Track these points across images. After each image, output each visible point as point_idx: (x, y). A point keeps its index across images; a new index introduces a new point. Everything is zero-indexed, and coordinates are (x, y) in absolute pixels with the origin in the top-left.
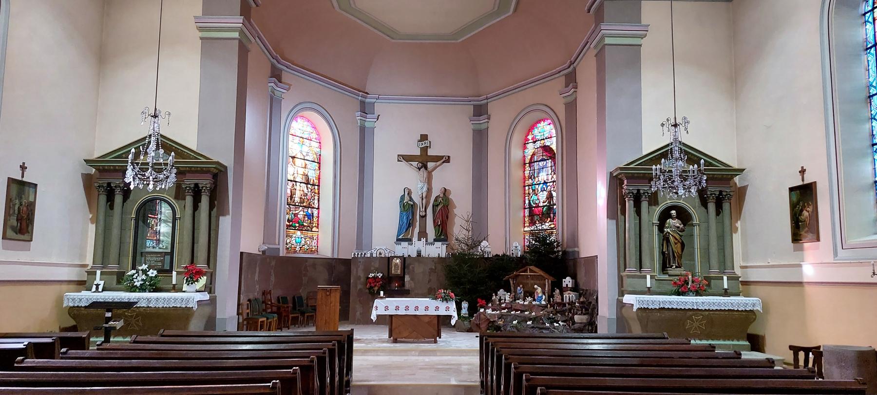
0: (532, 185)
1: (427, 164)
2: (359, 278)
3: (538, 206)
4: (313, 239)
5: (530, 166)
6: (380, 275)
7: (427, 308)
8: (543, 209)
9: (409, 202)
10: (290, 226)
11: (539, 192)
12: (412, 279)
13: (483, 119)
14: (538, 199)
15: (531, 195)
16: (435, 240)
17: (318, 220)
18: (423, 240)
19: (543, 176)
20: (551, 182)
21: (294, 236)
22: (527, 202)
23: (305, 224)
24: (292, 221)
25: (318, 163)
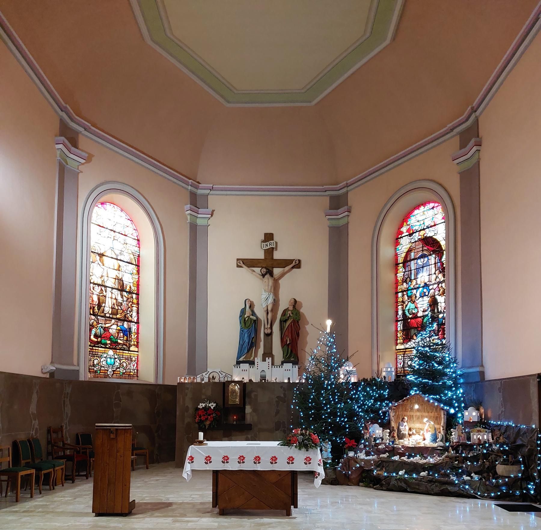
0: (408, 290)
1: (273, 270)
2: (187, 409)
3: (415, 316)
4: (131, 360)
5: (404, 267)
6: (212, 405)
7: (274, 460)
8: (423, 319)
9: (251, 317)
10: (98, 343)
11: (417, 298)
12: (255, 410)
13: (342, 212)
14: (416, 308)
15: (406, 303)
16: (283, 363)
17: (137, 338)
18: (269, 360)
19: (423, 277)
20: (435, 283)
21: (105, 355)
22: (400, 312)
23: (119, 341)
24: (100, 337)
25: (136, 265)
